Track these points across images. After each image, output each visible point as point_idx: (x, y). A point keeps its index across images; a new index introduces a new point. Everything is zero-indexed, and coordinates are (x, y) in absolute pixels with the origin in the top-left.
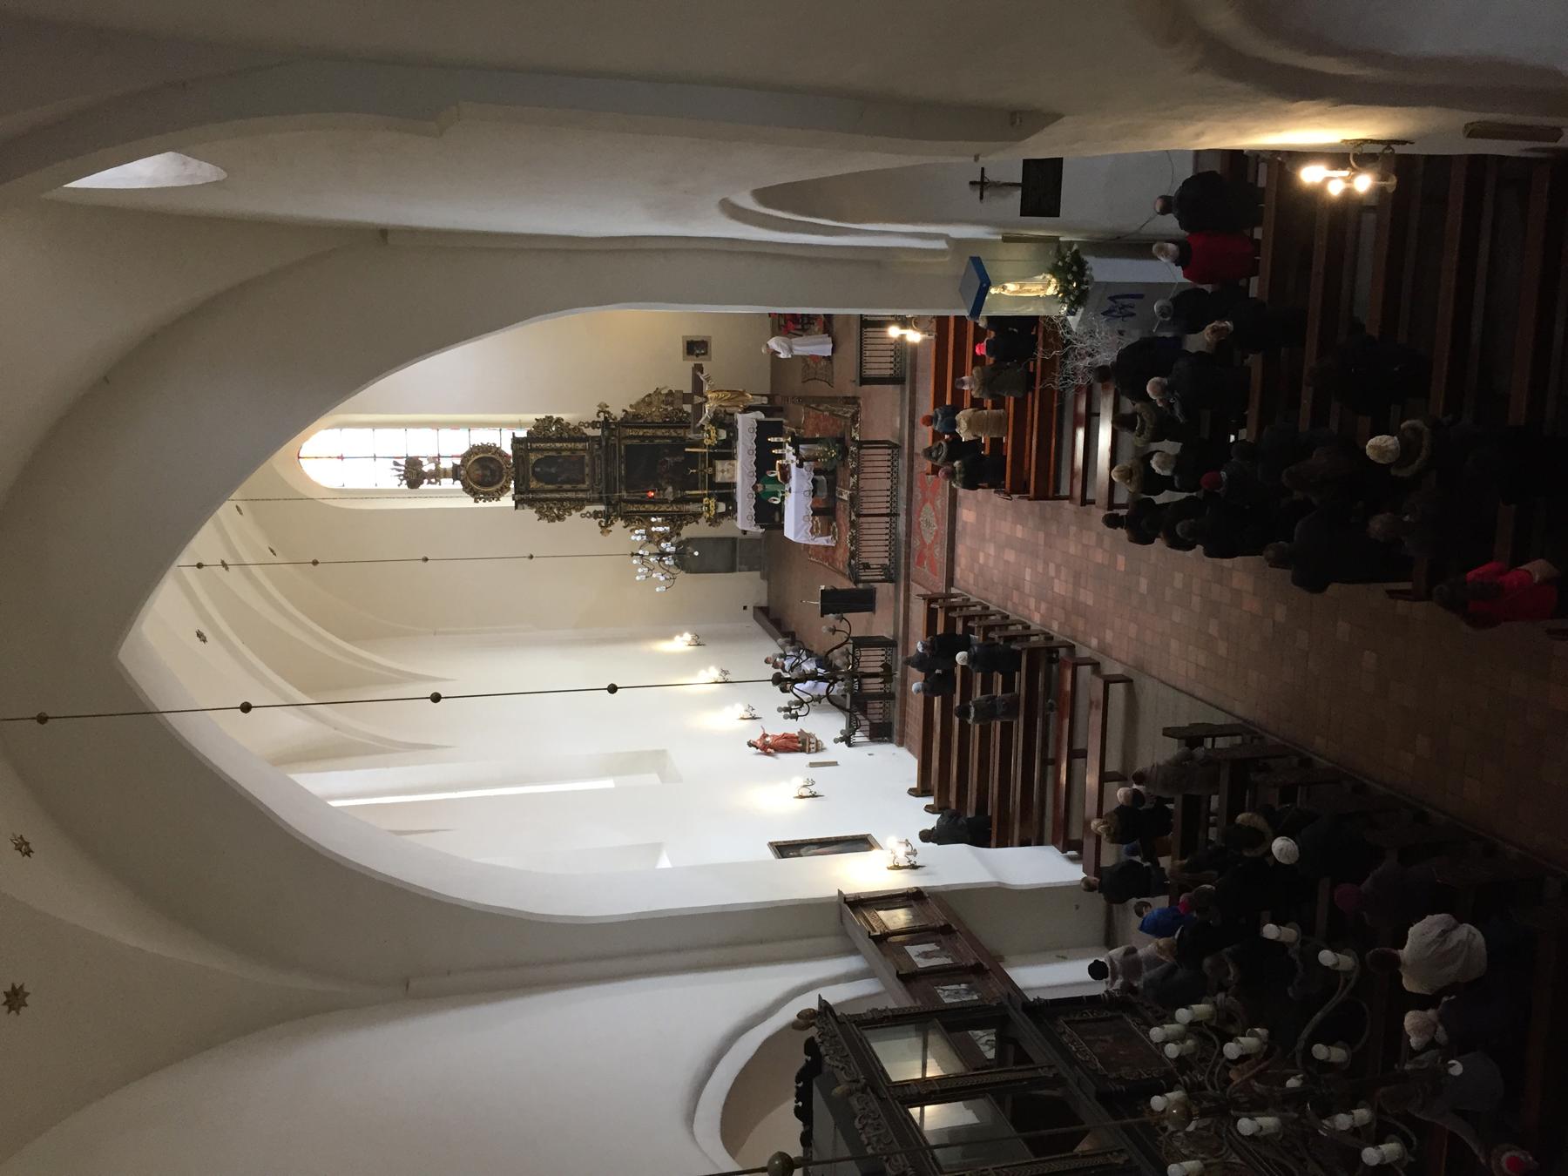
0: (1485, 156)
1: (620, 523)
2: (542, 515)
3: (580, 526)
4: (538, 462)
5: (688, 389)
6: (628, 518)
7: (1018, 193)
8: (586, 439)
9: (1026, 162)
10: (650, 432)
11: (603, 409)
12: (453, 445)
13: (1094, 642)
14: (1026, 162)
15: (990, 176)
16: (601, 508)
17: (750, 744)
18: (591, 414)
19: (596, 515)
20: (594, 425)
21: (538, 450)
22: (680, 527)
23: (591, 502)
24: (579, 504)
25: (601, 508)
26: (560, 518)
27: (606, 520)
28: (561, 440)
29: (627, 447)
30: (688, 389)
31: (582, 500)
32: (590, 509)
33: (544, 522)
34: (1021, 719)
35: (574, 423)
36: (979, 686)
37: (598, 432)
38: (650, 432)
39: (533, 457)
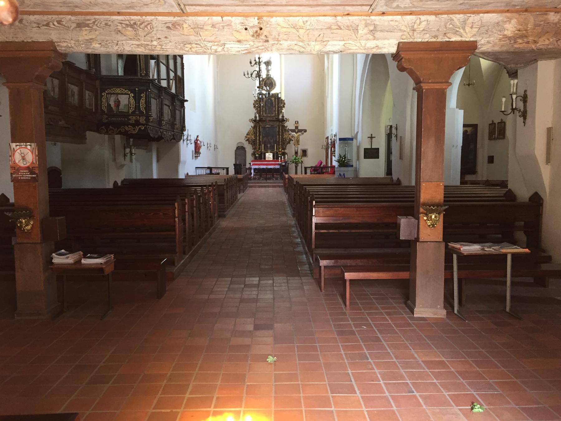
0: (445, 259)
1: (253, 125)
3: (252, 113)
4: (272, 100)
5: (299, 128)
6: (255, 127)
8: (279, 115)
9: (378, 158)
10: (281, 134)
11: (287, 120)
12: (275, 74)
13: (478, 409)
14: (378, 158)
15: (373, 139)
16: (258, 119)
17: (197, 136)
18: (286, 116)
19: (256, 117)
20: (283, 116)
21: (275, 100)
22: (251, 144)
23: (259, 116)
24: (259, 112)
25: (258, 119)
26: (255, 107)
27: (254, 121)
28: (278, 107)
29: (255, 169)
30: (299, 128)
31: (260, 113)
32: (257, 115)
33: (253, 102)
34: (313, 233)
35: (283, 111)
37: (280, 117)
38: (281, 134)
39: (273, 99)
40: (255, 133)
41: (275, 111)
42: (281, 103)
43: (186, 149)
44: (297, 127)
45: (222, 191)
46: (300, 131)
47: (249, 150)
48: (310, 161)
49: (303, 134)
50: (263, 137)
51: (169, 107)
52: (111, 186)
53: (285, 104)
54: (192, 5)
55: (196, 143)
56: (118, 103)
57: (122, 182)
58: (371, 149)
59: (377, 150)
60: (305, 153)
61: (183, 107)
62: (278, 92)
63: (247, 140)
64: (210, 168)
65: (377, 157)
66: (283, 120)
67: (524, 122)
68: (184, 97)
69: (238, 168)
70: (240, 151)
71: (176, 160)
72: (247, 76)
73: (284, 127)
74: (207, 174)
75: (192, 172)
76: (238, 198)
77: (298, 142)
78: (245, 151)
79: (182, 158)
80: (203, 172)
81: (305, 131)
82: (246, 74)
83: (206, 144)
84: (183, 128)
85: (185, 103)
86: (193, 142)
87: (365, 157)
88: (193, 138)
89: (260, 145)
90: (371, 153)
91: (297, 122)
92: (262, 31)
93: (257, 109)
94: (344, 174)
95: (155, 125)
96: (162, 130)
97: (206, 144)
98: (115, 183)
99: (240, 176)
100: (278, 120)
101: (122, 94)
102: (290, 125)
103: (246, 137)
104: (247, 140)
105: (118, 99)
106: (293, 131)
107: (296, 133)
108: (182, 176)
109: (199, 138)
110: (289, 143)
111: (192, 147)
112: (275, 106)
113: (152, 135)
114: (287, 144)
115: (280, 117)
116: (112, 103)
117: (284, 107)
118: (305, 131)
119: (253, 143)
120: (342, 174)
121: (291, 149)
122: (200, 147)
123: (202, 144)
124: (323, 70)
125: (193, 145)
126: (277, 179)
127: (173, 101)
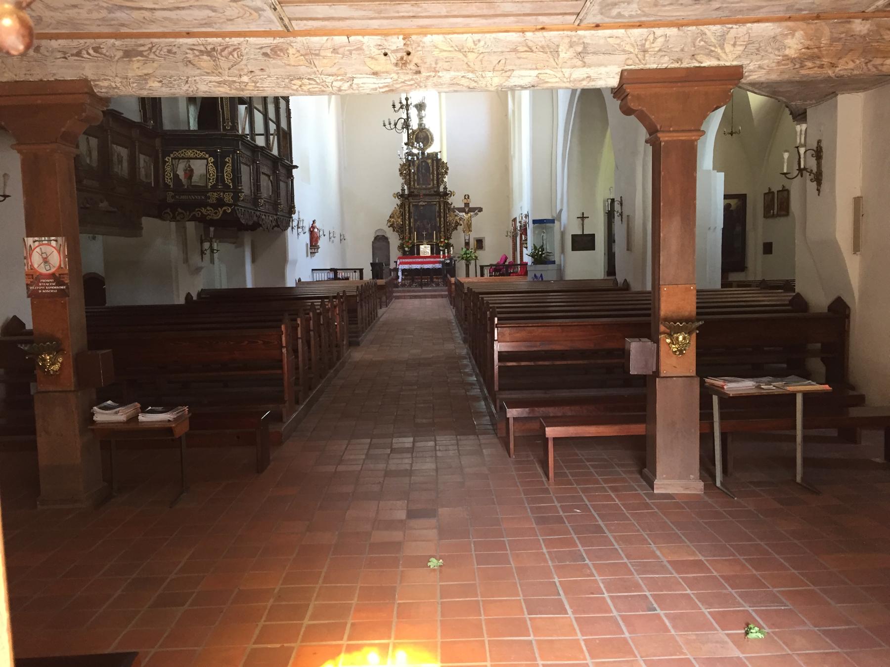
1: (399, 202)
2: (402, 166)
3: (397, 184)
6: (402, 206)
7: (580, 233)
8: (438, 187)
10: (442, 215)
11: (452, 194)
12: (432, 123)
15: (586, 221)
16: (406, 192)
17: (314, 222)
19: (403, 190)
20: (445, 188)
22: (397, 231)
23: (409, 188)
24: (408, 183)
25: (406, 192)
26: (401, 174)
27: (401, 196)
28: (438, 174)
31: (410, 184)
32: (406, 187)
33: (399, 167)
36: (243, 661)
37: (441, 189)
38: (442, 215)
39: (429, 161)
40: (403, 215)
41: (433, 180)
42: (443, 168)
43: (296, 242)
44: (467, 205)
45: (353, 305)
46: (473, 210)
47: (395, 241)
48: (489, 257)
49: (476, 214)
50: (415, 221)
51: (269, 176)
52: (181, 301)
53: (447, 169)
54: (301, 19)
55: (312, 232)
56: (190, 172)
57: (199, 294)
58: (583, 235)
59: (592, 236)
60: (480, 243)
61: (290, 176)
62: (437, 150)
63: (391, 226)
64: (335, 271)
65: (593, 248)
66: (446, 194)
67: (818, 190)
68: (292, 162)
69: (378, 269)
70: (380, 242)
71: (282, 259)
72: (388, 126)
73: (447, 204)
74: (329, 279)
75: (306, 277)
76: (379, 315)
77: (469, 227)
78: (388, 243)
79: (291, 255)
80: (324, 276)
81: (480, 210)
82: (387, 123)
83: (327, 233)
84: (291, 209)
85: (294, 171)
86: (307, 230)
87: (573, 249)
88: (307, 225)
89: (410, 233)
90: (583, 242)
91: (467, 197)
92: (410, 57)
93: (405, 178)
94: (541, 276)
95: (249, 205)
96: (258, 213)
97: (327, 233)
98: (188, 296)
99: (380, 282)
100: (437, 193)
101: (196, 158)
102: (456, 201)
103: (389, 221)
104: (391, 226)
105: (190, 166)
106: (461, 210)
107: (467, 213)
108: (290, 283)
109: (317, 224)
110: (456, 228)
111: (306, 238)
112: (433, 173)
113: (243, 222)
114: (453, 230)
115: (441, 189)
116: (181, 173)
117: (446, 173)
118: (480, 210)
119: (400, 229)
120: (538, 275)
121: (458, 239)
122: (318, 238)
123: (321, 233)
124: (507, 115)
125: (308, 235)
126: (437, 285)
127: (275, 168)
